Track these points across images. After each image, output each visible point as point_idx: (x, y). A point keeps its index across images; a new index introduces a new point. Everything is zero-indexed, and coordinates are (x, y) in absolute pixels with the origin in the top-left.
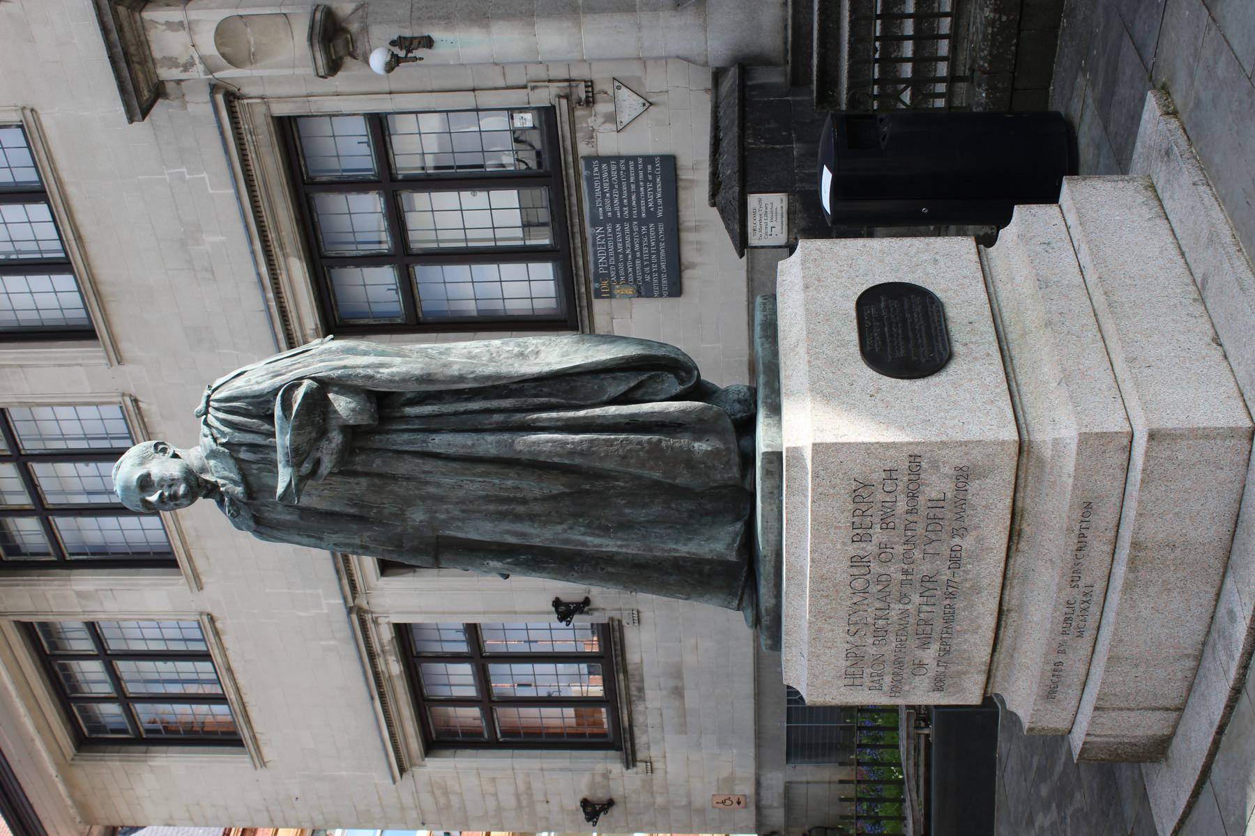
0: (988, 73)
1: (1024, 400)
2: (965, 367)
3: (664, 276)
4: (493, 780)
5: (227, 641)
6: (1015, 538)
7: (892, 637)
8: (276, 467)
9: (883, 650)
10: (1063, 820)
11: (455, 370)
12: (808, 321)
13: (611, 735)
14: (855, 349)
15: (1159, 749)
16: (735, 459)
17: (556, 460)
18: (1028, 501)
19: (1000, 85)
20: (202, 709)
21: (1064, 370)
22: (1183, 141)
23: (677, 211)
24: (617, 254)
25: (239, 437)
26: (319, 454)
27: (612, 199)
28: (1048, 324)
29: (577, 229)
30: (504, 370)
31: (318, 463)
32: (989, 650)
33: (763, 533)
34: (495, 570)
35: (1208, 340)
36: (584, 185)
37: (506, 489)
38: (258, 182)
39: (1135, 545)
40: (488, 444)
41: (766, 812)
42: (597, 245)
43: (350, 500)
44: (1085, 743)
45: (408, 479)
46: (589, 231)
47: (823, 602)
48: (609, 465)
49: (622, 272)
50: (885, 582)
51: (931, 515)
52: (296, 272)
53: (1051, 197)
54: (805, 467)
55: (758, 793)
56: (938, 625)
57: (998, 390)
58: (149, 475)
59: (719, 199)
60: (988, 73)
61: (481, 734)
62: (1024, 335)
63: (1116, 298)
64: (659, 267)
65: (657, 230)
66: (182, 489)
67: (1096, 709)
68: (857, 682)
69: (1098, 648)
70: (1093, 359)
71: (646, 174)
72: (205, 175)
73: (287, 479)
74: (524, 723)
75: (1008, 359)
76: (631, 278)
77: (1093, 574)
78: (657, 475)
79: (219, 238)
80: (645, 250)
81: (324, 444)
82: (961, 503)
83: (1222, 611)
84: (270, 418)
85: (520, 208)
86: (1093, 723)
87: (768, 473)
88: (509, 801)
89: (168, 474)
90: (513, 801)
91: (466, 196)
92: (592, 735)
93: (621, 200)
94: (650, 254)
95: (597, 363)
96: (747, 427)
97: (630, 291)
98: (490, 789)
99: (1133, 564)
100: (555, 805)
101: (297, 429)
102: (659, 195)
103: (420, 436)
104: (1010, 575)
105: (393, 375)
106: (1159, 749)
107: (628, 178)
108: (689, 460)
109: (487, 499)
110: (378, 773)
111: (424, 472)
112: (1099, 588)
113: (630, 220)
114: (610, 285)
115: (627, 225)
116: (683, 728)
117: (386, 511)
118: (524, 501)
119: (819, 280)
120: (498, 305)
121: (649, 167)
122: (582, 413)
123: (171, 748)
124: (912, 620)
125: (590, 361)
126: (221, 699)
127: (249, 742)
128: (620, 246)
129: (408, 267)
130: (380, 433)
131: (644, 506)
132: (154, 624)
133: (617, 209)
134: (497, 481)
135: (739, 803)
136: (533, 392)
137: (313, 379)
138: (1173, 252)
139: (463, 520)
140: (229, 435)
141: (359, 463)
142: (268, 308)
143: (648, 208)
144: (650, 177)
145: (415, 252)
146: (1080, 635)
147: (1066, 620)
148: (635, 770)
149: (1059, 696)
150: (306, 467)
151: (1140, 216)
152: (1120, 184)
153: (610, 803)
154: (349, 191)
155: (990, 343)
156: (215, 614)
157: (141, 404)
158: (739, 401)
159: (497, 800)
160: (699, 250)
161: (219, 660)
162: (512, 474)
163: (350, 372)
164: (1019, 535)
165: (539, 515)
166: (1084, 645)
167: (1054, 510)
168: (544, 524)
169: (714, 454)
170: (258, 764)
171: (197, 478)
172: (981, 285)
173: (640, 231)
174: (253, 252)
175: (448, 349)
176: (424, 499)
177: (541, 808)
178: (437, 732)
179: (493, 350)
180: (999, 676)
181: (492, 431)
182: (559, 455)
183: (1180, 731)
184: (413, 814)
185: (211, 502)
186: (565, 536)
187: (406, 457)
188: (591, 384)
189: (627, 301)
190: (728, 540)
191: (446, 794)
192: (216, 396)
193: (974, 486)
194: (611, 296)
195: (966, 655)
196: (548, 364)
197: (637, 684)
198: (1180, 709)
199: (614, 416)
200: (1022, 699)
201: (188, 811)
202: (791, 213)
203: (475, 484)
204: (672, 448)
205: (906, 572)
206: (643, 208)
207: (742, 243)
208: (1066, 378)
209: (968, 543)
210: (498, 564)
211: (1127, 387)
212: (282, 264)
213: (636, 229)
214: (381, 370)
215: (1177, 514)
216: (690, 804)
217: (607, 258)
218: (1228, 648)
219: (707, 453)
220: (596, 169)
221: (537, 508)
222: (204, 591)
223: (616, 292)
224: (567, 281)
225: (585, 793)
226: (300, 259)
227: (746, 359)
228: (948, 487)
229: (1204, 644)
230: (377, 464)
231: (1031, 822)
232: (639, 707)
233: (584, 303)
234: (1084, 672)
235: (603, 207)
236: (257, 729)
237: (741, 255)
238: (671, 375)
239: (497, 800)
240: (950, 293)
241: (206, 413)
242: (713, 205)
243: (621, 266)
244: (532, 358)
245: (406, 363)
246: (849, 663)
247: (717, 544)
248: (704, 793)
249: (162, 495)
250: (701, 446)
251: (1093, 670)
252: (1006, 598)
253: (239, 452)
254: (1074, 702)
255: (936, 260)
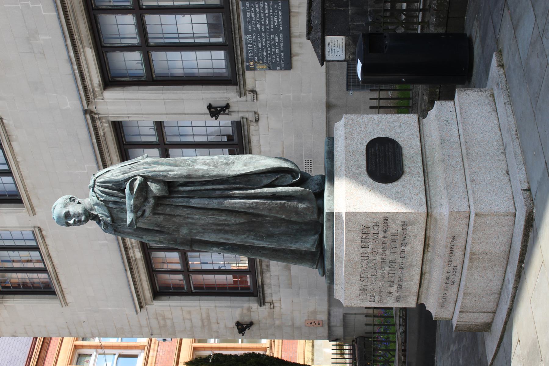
0: (437, 11)
1: (431, 193)
2: (408, 178)
3: (283, 60)
4: (190, 312)
5: (48, 241)
6: (426, 247)
7: (378, 282)
8: (126, 213)
9: (375, 287)
10: (459, 349)
11: (200, 173)
12: (346, 155)
13: (252, 288)
14: (364, 169)
15: (488, 327)
16: (316, 211)
17: (242, 210)
18: (431, 233)
19: (442, 16)
20: (35, 275)
21: (446, 183)
22: (504, 81)
23: (290, 27)
24: (258, 49)
25: (109, 198)
26: (145, 208)
27: (256, 21)
28: (443, 161)
29: (237, 36)
30: (221, 173)
31: (144, 211)
32: (418, 287)
33: (326, 242)
34: (216, 251)
35: (504, 172)
36: (241, 14)
37: (221, 220)
38: (69, 9)
39: (472, 253)
40: (214, 203)
41: (334, 329)
42: (247, 43)
43: (156, 224)
44: (457, 324)
45: (180, 216)
46: (244, 37)
47: (350, 269)
48: (265, 213)
49: (260, 58)
50: (375, 263)
51: (393, 238)
52: (89, 55)
53: (451, 97)
54: (343, 220)
55: (329, 319)
56: (397, 278)
57: (421, 189)
58: (68, 212)
59: (311, 36)
60: (437, 11)
61: (183, 288)
62: (433, 163)
63: (470, 151)
64: (280, 55)
65: (279, 37)
66: (83, 218)
67: (460, 312)
68: (365, 298)
69: (460, 289)
70: (459, 178)
71: (273, 9)
72: (40, 5)
73: (131, 218)
74: (207, 282)
75: (426, 174)
76: (265, 60)
77: (457, 262)
78: (283, 217)
79: (47, 37)
80: (273, 47)
81: (147, 204)
82: (404, 234)
83: (506, 278)
84: (123, 191)
85: (208, 24)
86: (459, 317)
87: (328, 220)
88: (197, 322)
89: (77, 211)
90: (200, 323)
91: (179, 17)
92: (242, 289)
93: (260, 22)
94: (276, 49)
95: (259, 170)
96: (320, 195)
97: (265, 67)
98: (188, 317)
99: (471, 260)
100: (222, 325)
101: (136, 198)
102: (280, 20)
103: (186, 200)
104: (425, 260)
105: (174, 175)
106: (488, 327)
107: (264, 10)
108: (296, 211)
109: (213, 224)
110: (127, 307)
111: (188, 214)
112: (459, 267)
113: (265, 32)
114: (254, 64)
115: (263, 35)
116: (290, 286)
117: (172, 229)
118: (228, 225)
119: (351, 135)
120: (196, 71)
121: (275, 6)
122: (253, 191)
123: (16, 296)
124: (386, 276)
125: (256, 169)
126: (44, 270)
127: (59, 293)
128: (259, 44)
129: (148, 52)
130: (169, 198)
131: (278, 227)
132: (8, 232)
133: (258, 26)
134: (217, 217)
135: (319, 324)
136: (233, 181)
137: (141, 176)
138: (496, 129)
139: (203, 233)
140: (104, 197)
141: (160, 209)
142: (74, 73)
143: (274, 26)
144: (276, 11)
145: (152, 44)
146: (453, 284)
147: (447, 278)
148: (264, 307)
149: (446, 306)
150: (139, 213)
151: (486, 110)
152: (480, 93)
153: (251, 324)
154: (117, 14)
155: (419, 167)
156: (42, 227)
157: (4, 121)
158: (317, 184)
159: (191, 322)
160: (301, 47)
161: (44, 251)
162: (224, 215)
163: (157, 173)
164: (428, 246)
165: (235, 231)
166: (455, 288)
167: (441, 238)
168: (237, 235)
169: (307, 209)
170: (63, 304)
171: (89, 213)
172: (419, 139)
173: (270, 37)
174: (67, 46)
175: (196, 160)
176: (186, 224)
177: (214, 327)
178: (159, 287)
179: (215, 161)
180: (423, 296)
181: (216, 198)
182: (243, 208)
183: (494, 321)
184: (146, 330)
185: (94, 222)
186: (245, 240)
187: (180, 208)
188: (258, 179)
189: (263, 72)
190: (312, 243)
191: (164, 319)
192: (98, 180)
193: (409, 228)
194: (255, 69)
195: (408, 289)
196: (239, 171)
197: (266, 263)
198: (494, 313)
199: (266, 193)
200: (432, 306)
201: (25, 329)
202: (347, 45)
203: (208, 219)
204: (290, 206)
205: (383, 259)
206: (272, 26)
207: (322, 59)
208: (447, 187)
209: (407, 249)
210: (217, 249)
211: (470, 192)
212: (82, 51)
213: (268, 36)
214: (170, 173)
215: (487, 242)
216: (293, 324)
217: (253, 50)
218: (507, 292)
219: (304, 209)
220: (248, 6)
221: (234, 228)
222: (36, 216)
223: (257, 67)
224: (232, 60)
225: (238, 318)
226: (91, 48)
227: (324, 101)
228: (399, 229)
229: (501, 289)
230: (168, 210)
231: (449, 348)
232: (267, 275)
233: (241, 73)
234: (455, 297)
235: (251, 25)
236: (64, 285)
237: (322, 65)
238: (289, 175)
239: (191, 322)
240: (405, 142)
241: (94, 187)
242: (308, 39)
243: (260, 54)
244: (231, 165)
245: (180, 170)
246: (361, 292)
247: (307, 244)
248: (300, 318)
249: (75, 220)
250: (302, 206)
251: (459, 297)
252: (424, 268)
253: (108, 204)
254: (453, 308)
255: (401, 126)
